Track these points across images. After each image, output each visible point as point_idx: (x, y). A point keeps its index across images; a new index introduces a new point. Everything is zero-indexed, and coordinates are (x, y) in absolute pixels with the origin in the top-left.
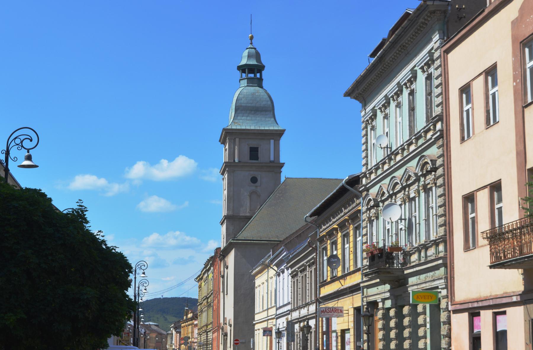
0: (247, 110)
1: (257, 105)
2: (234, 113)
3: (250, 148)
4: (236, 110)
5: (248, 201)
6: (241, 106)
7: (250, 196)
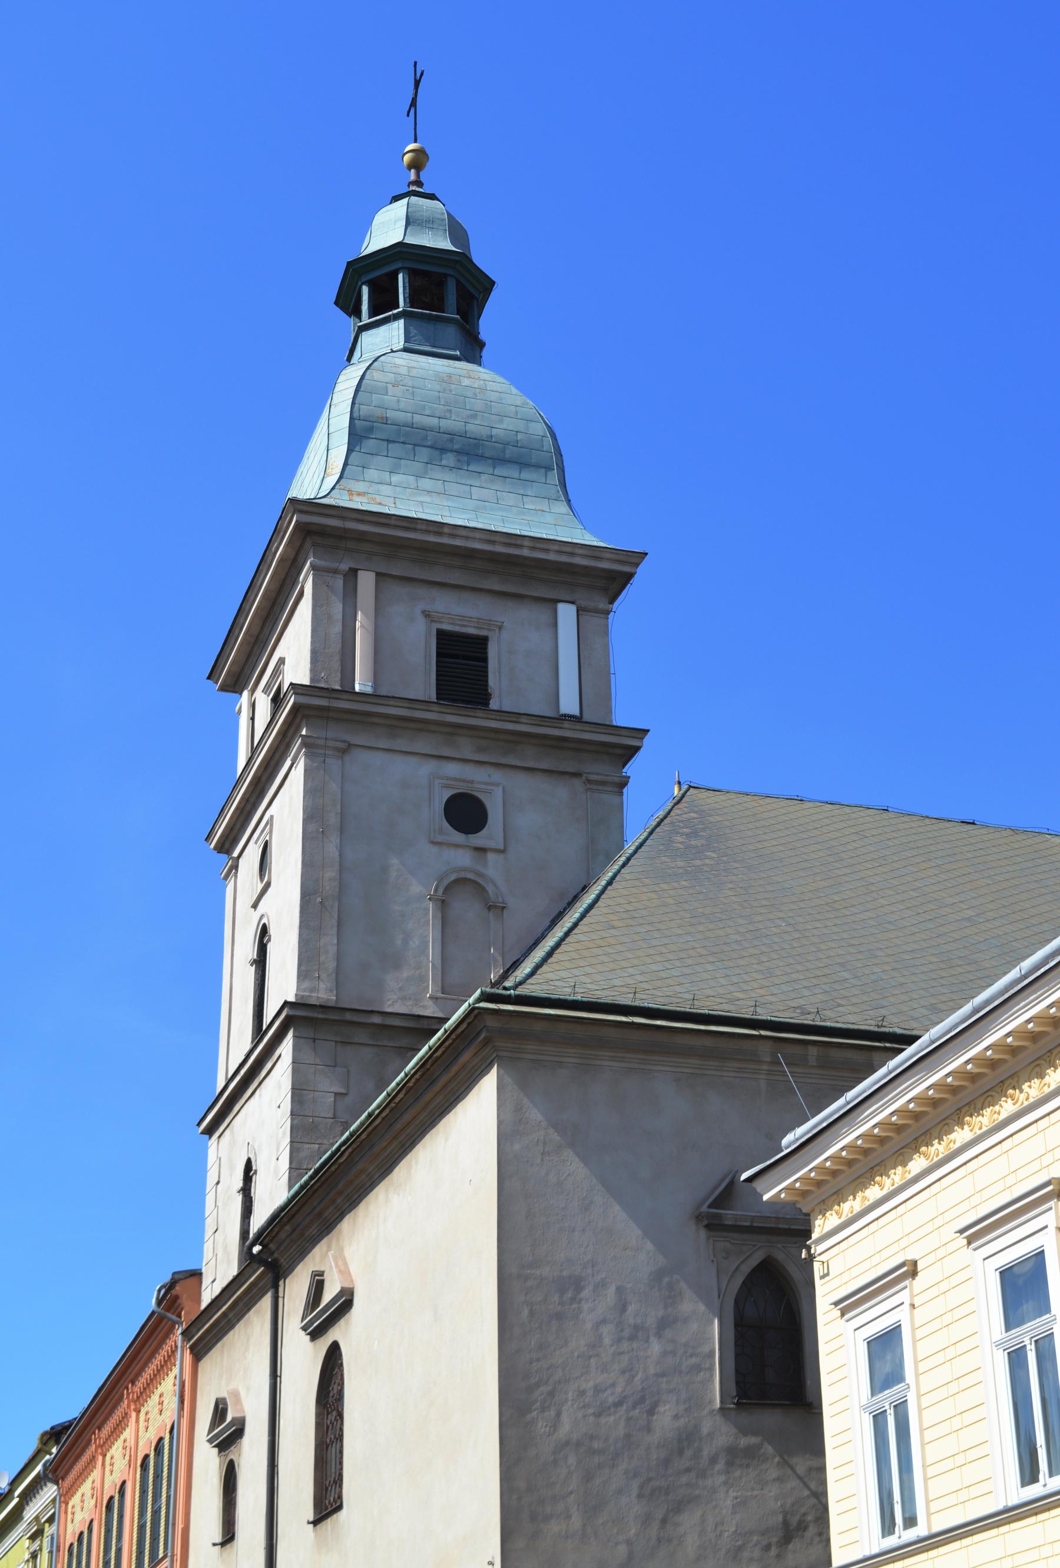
0: (415, 445)
1: (470, 428)
2: (344, 449)
3: (441, 634)
4: (357, 435)
5: (432, 934)
6: (385, 421)
7: (443, 904)
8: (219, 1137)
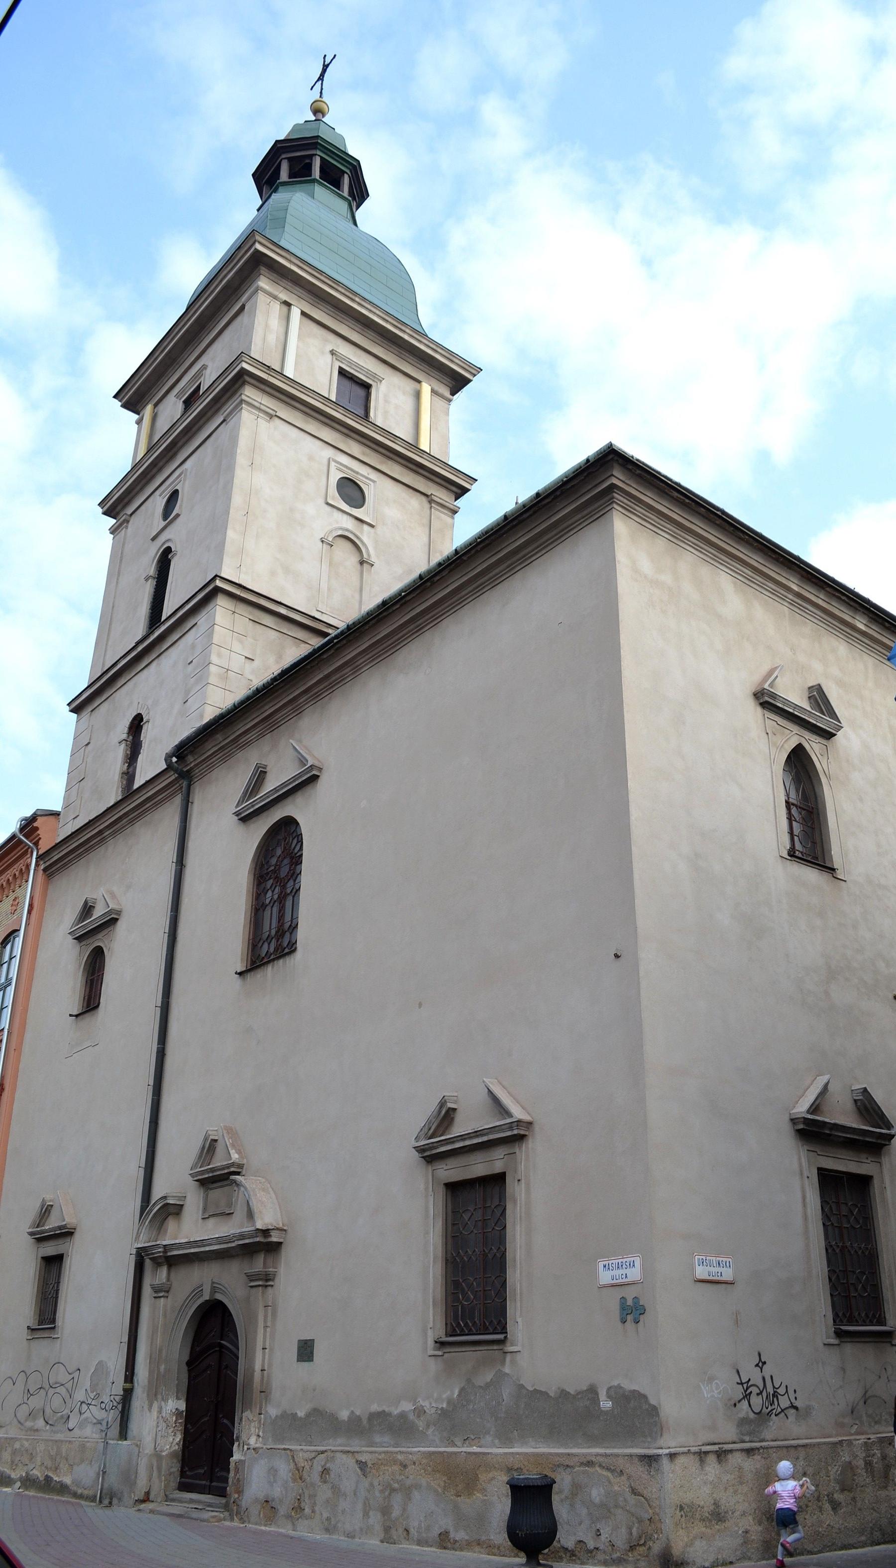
8: (92, 711)
